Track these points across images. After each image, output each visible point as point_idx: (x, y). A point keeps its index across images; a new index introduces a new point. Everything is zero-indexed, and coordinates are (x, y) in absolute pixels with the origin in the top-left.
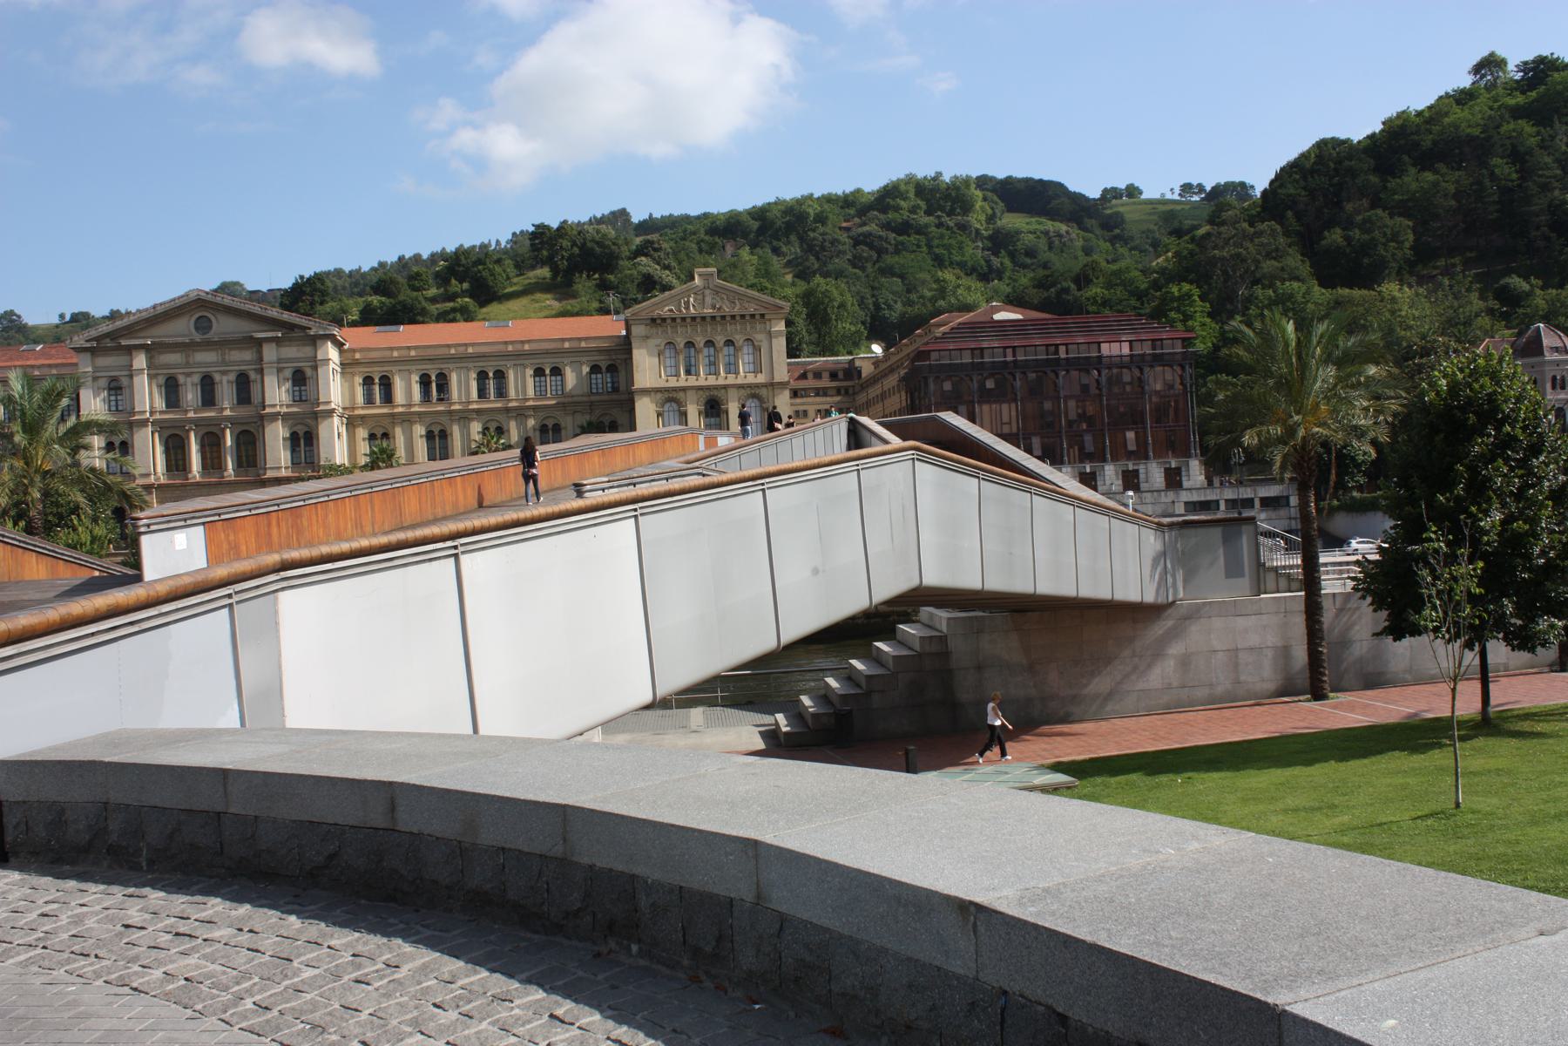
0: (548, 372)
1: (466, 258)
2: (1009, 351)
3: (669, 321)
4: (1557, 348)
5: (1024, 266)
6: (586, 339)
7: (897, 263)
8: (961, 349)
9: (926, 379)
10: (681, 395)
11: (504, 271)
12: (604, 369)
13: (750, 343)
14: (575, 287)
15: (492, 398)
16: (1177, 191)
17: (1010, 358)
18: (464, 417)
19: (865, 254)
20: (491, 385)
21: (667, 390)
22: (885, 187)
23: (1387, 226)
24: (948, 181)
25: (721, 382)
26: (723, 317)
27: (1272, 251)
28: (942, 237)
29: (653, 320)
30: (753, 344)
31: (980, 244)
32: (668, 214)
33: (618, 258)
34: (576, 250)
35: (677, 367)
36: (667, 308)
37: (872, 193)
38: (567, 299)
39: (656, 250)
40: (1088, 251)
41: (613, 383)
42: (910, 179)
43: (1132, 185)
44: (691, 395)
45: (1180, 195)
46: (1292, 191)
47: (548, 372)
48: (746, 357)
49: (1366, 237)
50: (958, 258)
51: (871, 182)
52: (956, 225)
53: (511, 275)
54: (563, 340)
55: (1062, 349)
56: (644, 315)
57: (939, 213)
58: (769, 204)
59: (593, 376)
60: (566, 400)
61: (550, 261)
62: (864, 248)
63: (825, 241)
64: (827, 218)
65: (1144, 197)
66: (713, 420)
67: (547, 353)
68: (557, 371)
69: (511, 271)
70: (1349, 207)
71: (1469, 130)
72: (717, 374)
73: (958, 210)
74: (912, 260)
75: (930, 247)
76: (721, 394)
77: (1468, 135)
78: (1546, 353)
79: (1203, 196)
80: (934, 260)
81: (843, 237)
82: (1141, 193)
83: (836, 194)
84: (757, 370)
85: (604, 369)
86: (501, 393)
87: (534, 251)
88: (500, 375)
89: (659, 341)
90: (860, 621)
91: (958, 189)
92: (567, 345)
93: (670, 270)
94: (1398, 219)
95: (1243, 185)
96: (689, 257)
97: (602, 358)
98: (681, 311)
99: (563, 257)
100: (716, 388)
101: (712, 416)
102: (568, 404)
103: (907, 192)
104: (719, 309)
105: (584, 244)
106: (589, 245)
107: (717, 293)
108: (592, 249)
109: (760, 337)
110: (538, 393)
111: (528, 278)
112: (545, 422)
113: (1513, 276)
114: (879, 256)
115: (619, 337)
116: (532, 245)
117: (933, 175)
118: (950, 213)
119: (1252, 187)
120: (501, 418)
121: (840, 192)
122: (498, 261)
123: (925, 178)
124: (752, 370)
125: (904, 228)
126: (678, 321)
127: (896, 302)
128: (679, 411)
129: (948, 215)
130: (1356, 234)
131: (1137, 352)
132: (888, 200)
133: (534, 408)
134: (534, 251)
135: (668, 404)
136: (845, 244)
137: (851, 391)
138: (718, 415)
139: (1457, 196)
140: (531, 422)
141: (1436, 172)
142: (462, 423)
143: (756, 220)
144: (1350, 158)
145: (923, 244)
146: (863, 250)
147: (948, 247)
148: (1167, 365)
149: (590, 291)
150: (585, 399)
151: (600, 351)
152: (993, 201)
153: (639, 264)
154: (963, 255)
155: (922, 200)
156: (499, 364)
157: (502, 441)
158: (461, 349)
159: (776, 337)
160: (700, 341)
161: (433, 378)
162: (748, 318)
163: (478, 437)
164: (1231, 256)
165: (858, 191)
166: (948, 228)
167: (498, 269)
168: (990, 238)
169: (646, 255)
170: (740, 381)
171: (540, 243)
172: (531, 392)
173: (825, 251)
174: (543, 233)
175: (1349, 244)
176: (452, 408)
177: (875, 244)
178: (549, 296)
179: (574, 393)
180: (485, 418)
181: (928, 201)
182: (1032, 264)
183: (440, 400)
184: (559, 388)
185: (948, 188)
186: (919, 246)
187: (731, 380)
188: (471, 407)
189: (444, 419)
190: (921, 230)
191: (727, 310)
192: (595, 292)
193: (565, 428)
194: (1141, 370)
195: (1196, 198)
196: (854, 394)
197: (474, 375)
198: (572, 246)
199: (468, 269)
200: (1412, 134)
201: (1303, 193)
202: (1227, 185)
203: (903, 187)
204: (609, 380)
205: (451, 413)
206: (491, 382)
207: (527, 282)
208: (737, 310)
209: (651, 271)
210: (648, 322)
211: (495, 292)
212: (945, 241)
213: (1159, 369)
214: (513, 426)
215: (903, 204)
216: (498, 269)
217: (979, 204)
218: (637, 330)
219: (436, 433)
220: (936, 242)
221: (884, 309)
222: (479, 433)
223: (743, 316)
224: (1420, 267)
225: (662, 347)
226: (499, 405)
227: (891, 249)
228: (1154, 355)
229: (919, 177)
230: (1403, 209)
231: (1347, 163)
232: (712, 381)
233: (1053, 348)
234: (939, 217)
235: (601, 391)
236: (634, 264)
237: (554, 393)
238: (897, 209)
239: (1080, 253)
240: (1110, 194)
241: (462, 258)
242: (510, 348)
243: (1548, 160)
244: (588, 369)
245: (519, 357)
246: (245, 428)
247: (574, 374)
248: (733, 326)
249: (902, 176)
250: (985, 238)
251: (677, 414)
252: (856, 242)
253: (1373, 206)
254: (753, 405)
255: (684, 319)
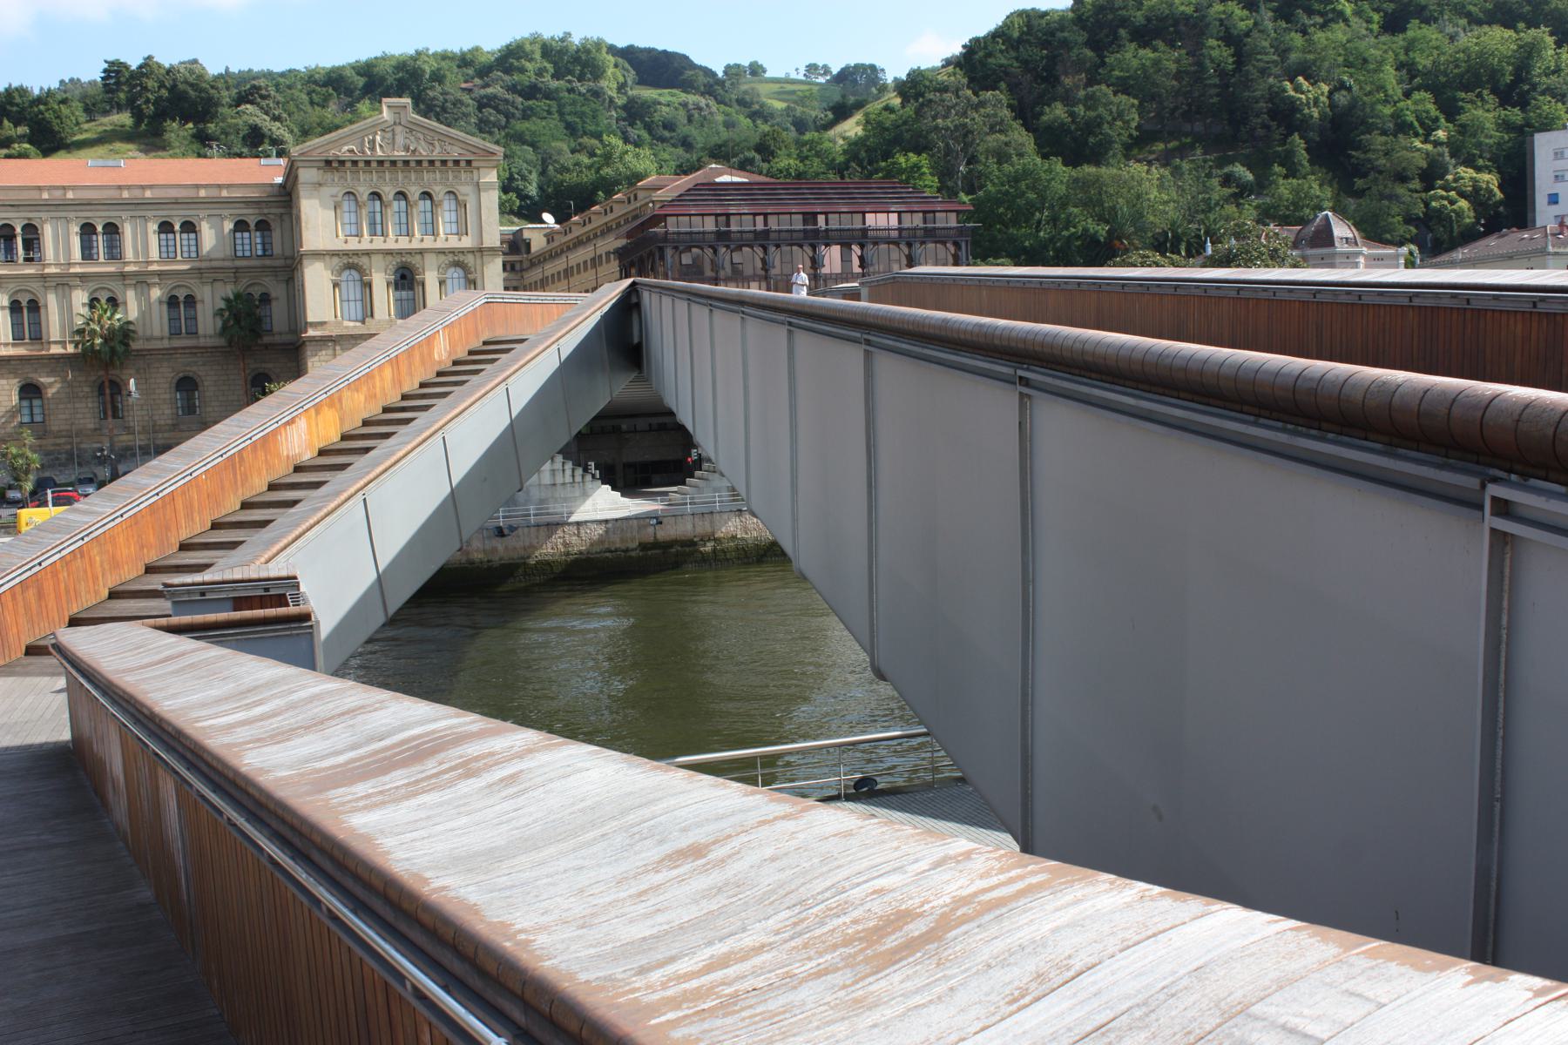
0: (177, 227)
1: (21, 96)
2: (760, 219)
3: (348, 165)
4: (1347, 239)
5: (663, 140)
6: (229, 186)
7: (527, 129)
8: (703, 215)
9: (661, 250)
10: (364, 261)
11: (73, 114)
12: (252, 226)
13: (352, 197)
14: (167, 136)
15: (102, 260)
16: (802, 71)
17: (760, 226)
18: (63, 283)
19: (492, 118)
20: (100, 241)
21: (346, 254)
22: (508, 47)
23: (1111, 103)
24: (577, 43)
25: (415, 245)
26: (419, 163)
27: (997, 124)
28: (574, 103)
29: (328, 163)
30: (456, 199)
31: (614, 113)
32: (246, 69)
33: (218, 104)
34: (165, 93)
35: (358, 225)
36: (346, 148)
37: (493, 53)
38: (156, 151)
39: (263, 97)
40: (729, 125)
41: (263, 244)
42: (535, 39)
43: (756, 62)
44: (377, 260)
45: (805, 75)
46: (1003, 61)
47: (177, 227)
48: (447, 214)
49: (1092, 114)
50: (593, 128)
51: (492, 42)
52: (588, 91)
53: (81, 119)
54: (198, 187)
55: (821, 219)
56: (315, 155)
57: (569, 77)
58: (376, 58)
59: (238, 235)
60: (204, 265)
61: (131, 105)
62: (491, 111)
63: (446, 101)
64: (444, 76)
65: (767, 75)
66: (404, 293)
67: (176, 202)
68: (189, 227)
69: (82, 117)
70: (1068, 81)
71: (1182, 8)
72: (410, 234)
73: (589, 76)
74: (544, 127)
75: (561, 114)
76: (415, 260)
77: (1183, 13)
78: (1337, 244)
79: (828, 78)
80: (566, 128)
81: (466, 98)
82: (765, 72)
83: (452, 52)
84: (462, 231)
85: (252, 226)
86: (114, 252)
87: (107, 92)
88: (112, 229)
89: (339, 191)
90: (633, 554)
91: (588, 52)
92: (202, 193)
93: (282, 123)
94: (1123, 98)
95: (873, 67)
96: (300, 109)
97: (251, 211)
98: (363, 152)
99: (148, 101)
100: (410, 252)
101: (403, 289)
102: (289, 269)
103: (533, 52)
104: (414, 151)
105: (174, 86)
106: (181, 87)
107: (411, 130)
108: (185, 92)
109: (465, 190)
110: (164, 255)
111: (101, 124)
112: (174, 293)
113: (1237, 164)
114: (508, 122)
115: (272, 185)
116: (105, 85)
117: (561, 35)
118: (581, 79)
119: (883, 70)
120: (116, 286)
121: (456, 50)
122: (64, 101)
123: (553, 38)
124: (454, 231)
125: (531, 92)
126: (361, 165)
127: (530, 172)
128: (361, 280)
129: (579, 81)
130: (1080, 110)
131: (907, 224)
132: (511, 60)
133: (160, 274)
134: (107, 92)
135: (346, 273)
136: (468, 105)
137: (518, 267)
138: (411, 288)
139: (1178, 76)
140: (156, 293)
141: (1155, 50)
142: (60, 291)
143: (362, 76)
144: (1062, 29)
145: (554, 110)
146: (490, 114)
147: (582, 115)
148: (794, 244)
149: (186, 142)
150: (227, 264)
151: (248, 203)
152: (623, 68)
153: (244, 113)
154: (597, 125)
155: (550, 62)
156: (112, 215)
157: (118, 316)
158: (58, 194)
159: (486, 190)
160: (388, 192)
161: (18, 230)
162: (450, 164)
163: (85, 311)
164: (956, 126)
165: (477, 49)
166: (580, 94)
167: (65, 110)
168: (624, 107)
169: (252, 103)
170: (440, 244)
171: (115, 83)
172: (154, 254)
173: (446, 112)
174: (118, 72)
175: (1073, 122)
176: (47, 271)
177: (501, 107)
178: (130, 146)
179: (213, 256)
180: (93, 285)
181: (555, 64)
182: (671, 138)
183: (28, 260)
184: (193, 249)
185: (578, 51)
186: (549, 112)
187: (429, 243)
188: (72, 270)
189: (35, 286)
190: (549, 95)
191: (424, 152)
192: (192, 142)
193: (203, 301)
194: (715, 252)
195: (821, 80)
196: (522, 270)
197: (75, 229)
198: (159, 88)
199: (23, 109)
200: (1120, 9)
201: (1016, 64)
202: (857, 67)
203: (528, 47)
204: (259, 240)
205: (44, 277)
206: (100, 238)
207: (101, 129)
208: (436, 155)
209: (258, 121)
210: (322, 164)
211: (62, 139)
212: (578, 109)
213: (931, 246)
214: (131, 295)
215: (528, 65)
216: (65, 110)
217: (610, 71)
218: (306, 175)
219: (24, 304)
220: (568, 109)
221: (517, 180)
222: (84, 305)
223: (444, 162)
224: (1135, 151)
225: (339, 199)
226: (111, 269)
227: (518, 114)
228: (925, 229)
229: (545, 37)
230: (1123, 87)
231: (1059, 35)
232: (404, 243)
233: (930, 216)
234: (569, 81)
235: (247, 254)
236: (237, 113)
237: (186, 255)
238: (522, 70)
239: (721, 128)
240: (733, 71)
241: (16, 95)
242: (126, 194)
243: (1266, 44)
244: (231, 226)
245: (138, 206)
246: (164, 219)
247: (213, 231)
248: (431, 175)
249: (527, 35)
250: (620, 108)
251: (358, 284)
252: (482, 104)
253: (1091, 82)
254: (456, 275)
255: (368, 163)
